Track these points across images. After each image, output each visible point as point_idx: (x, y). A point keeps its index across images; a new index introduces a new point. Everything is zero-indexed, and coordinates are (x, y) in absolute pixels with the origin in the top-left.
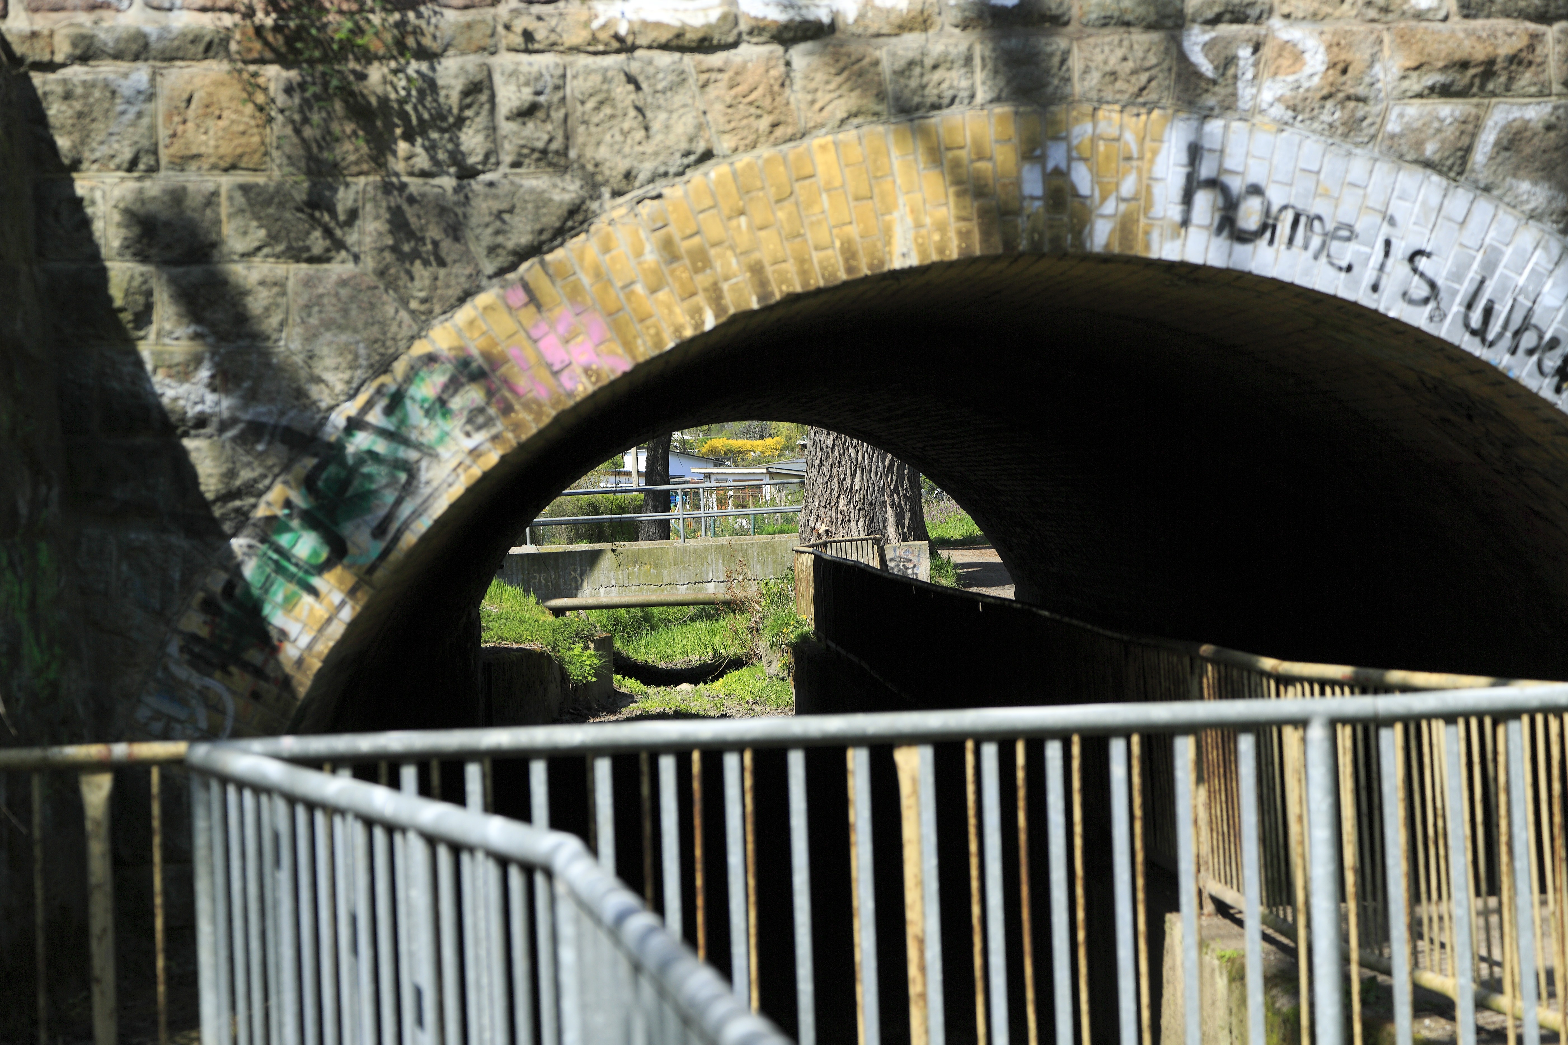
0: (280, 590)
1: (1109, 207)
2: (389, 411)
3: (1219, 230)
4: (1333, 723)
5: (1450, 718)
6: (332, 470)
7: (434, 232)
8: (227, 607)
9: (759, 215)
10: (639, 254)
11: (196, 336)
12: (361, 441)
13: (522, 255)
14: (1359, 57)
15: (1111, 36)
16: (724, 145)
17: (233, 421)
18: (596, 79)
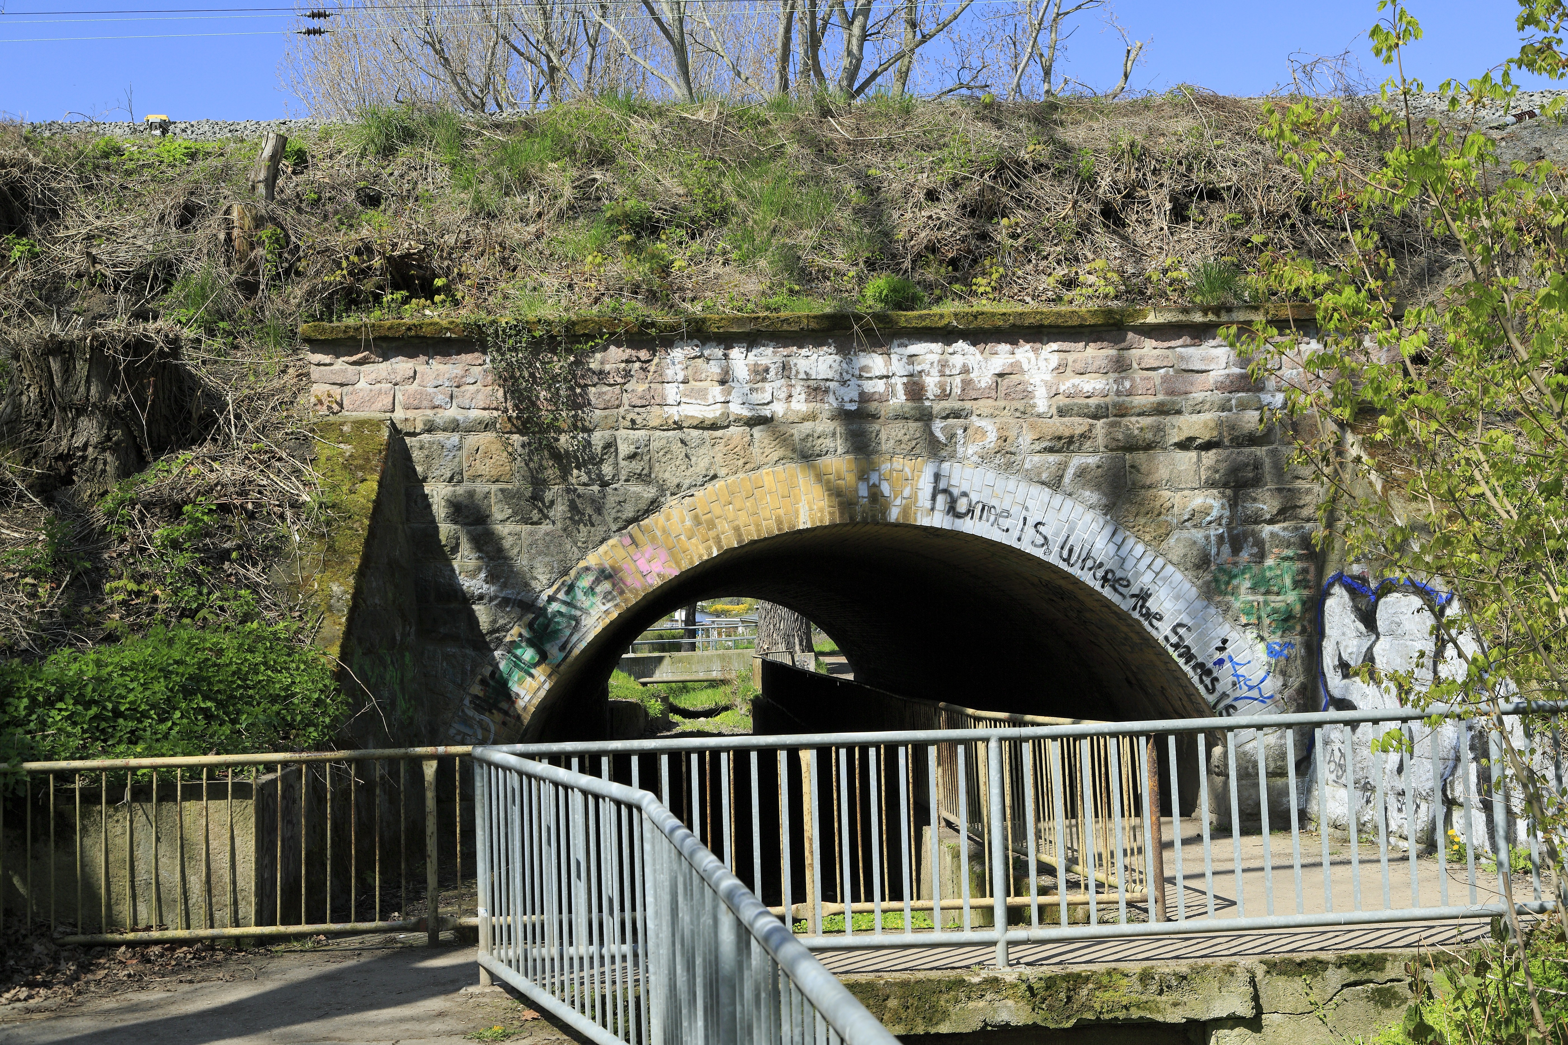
0: (517, 675)
1: (898, 502)
2: (568, 593)
3: (948, 513)
4: (1001, 740)
5: (1054, 738)
6: (541, 620)
7: (589, 511)
8: (492, 683)
9: (738, 504)
10: (683, 522)
11: (479, 558)
12: (555, 607)
13: (629, 522)
14: (1012, 434)
15: (900, 424)
16: (722, 472)
17: (496, 597)
18: (664, 442)
